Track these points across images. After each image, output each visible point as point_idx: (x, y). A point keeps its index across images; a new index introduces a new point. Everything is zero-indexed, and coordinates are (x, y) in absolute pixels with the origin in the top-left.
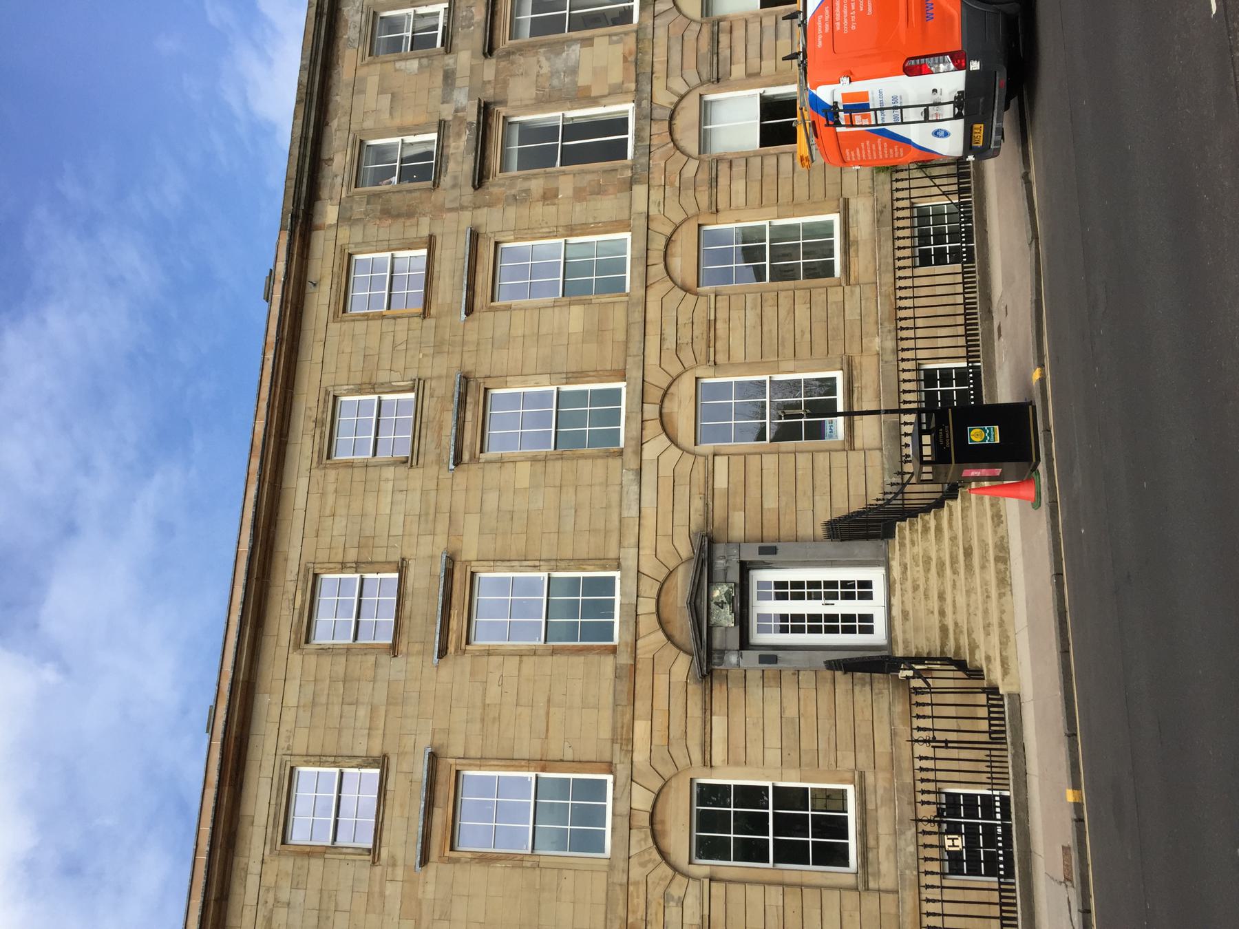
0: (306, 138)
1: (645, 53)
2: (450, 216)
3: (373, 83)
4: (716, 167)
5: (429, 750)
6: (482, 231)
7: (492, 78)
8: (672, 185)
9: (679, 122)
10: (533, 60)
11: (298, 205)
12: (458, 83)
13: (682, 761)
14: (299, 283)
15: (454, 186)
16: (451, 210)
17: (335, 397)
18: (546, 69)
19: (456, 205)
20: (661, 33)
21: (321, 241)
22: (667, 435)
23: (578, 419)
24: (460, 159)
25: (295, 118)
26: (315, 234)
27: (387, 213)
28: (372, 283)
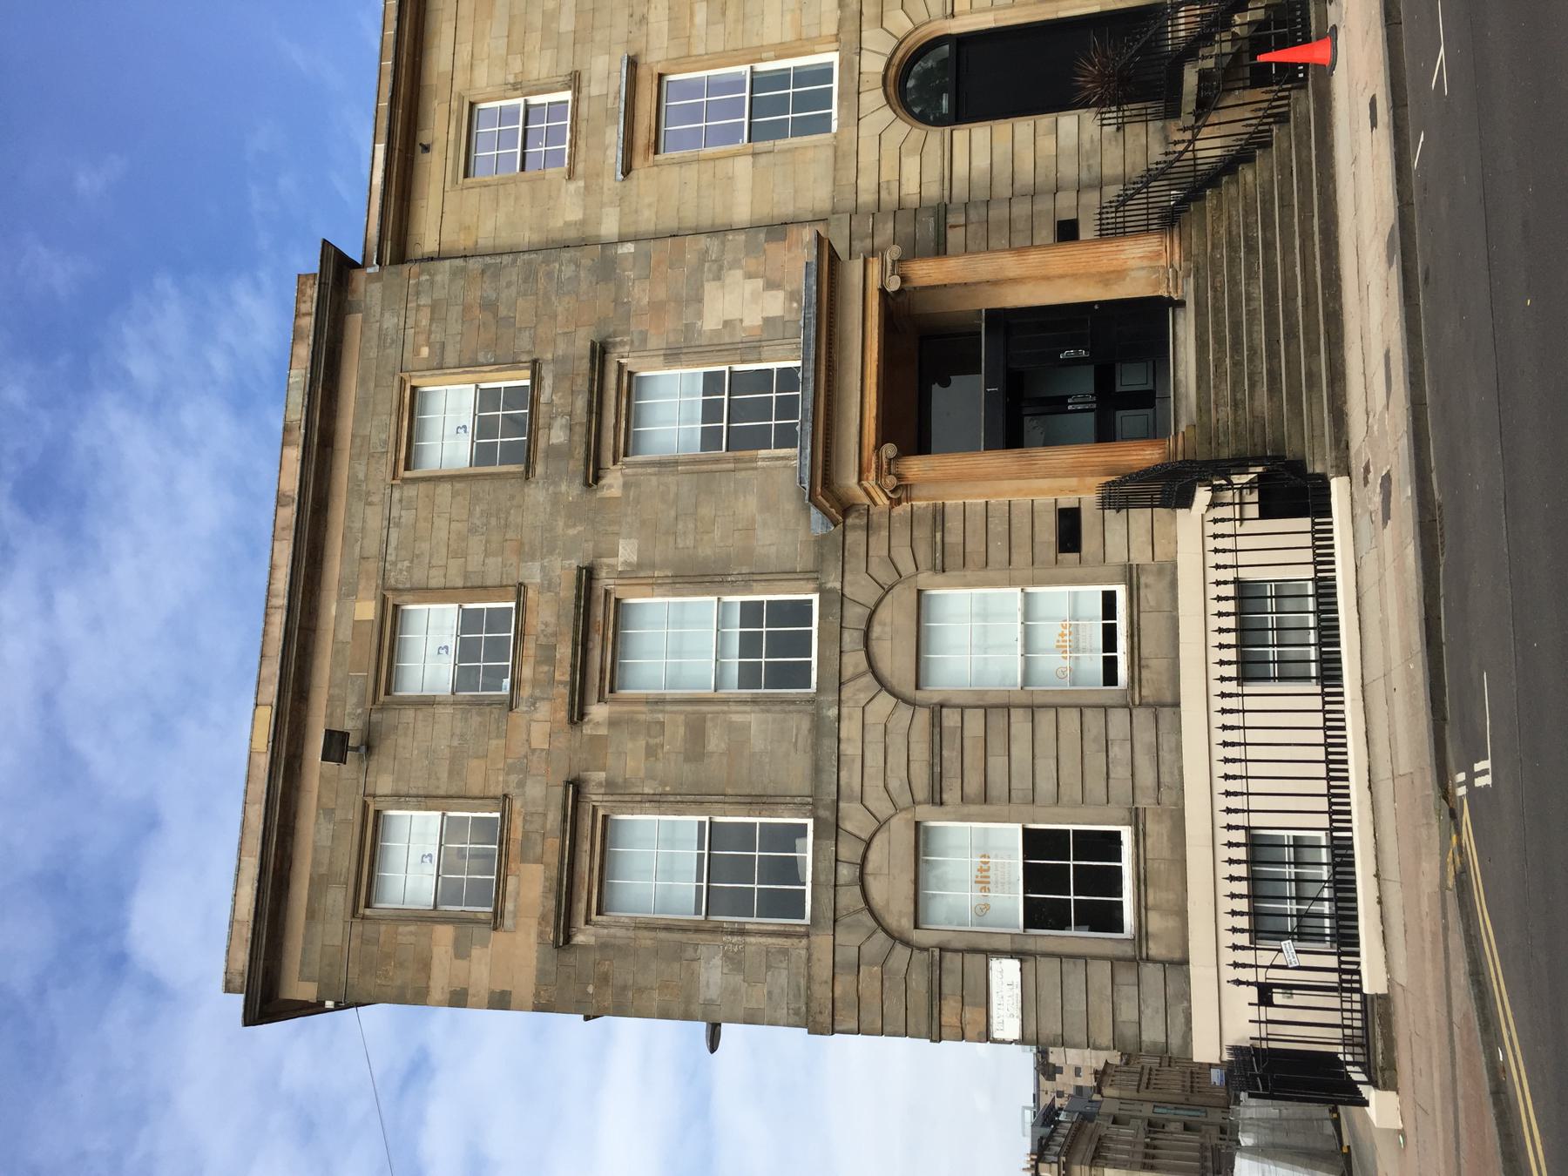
13: (906, 566)
14: (415, 39)
17: (472, 105)
23: (780, 105)
28: (502, 140)
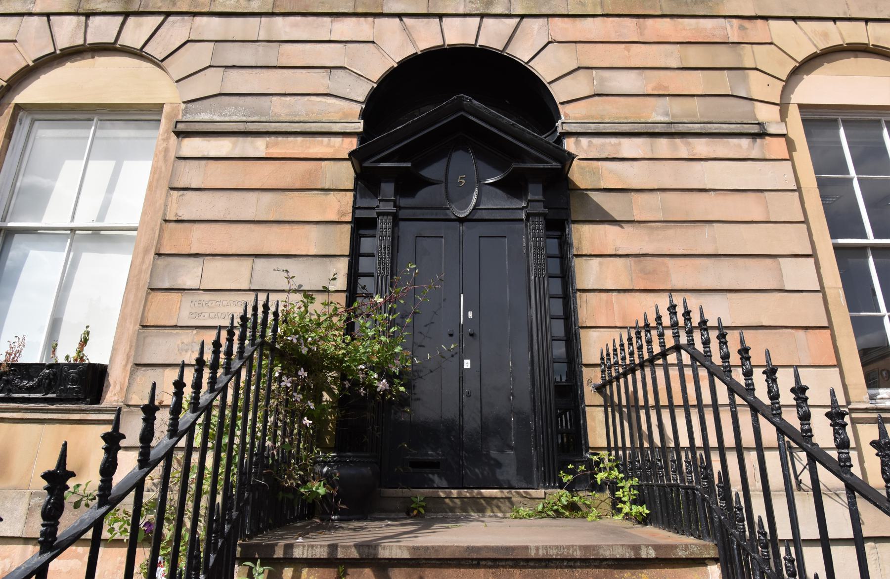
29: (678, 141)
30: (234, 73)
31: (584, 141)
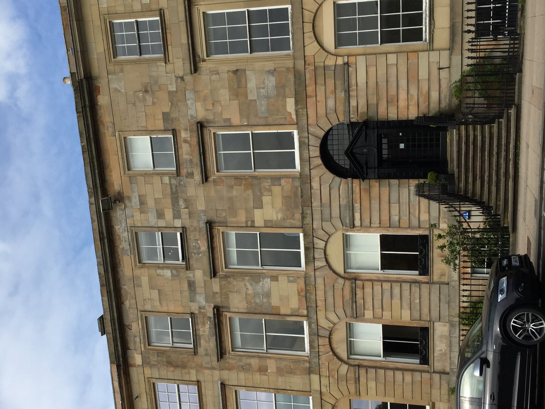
0: (114, 319)
1: (311, 294)
2: (207, 372)
3: (145, 280)
4: (359, 366)
5: (220, 382)
6: (227, 383)
7: (218, 291)
8: (333, 377)
9: (335, 337)
10: (242, 284)
11: (119, 359)
12: (198, 290)
15: (207, 355)
16: (207, 368)
18: (250, 291)
19: (209, 366)
20: (320, 281)
21: (136, 374)
22: (317, 42)
24: (207, 339)
25: (102, 296)
26: (131, 368)
27: (169, 363)
29: (350, 89)
30: (333, 215)
31: (352, 116)
